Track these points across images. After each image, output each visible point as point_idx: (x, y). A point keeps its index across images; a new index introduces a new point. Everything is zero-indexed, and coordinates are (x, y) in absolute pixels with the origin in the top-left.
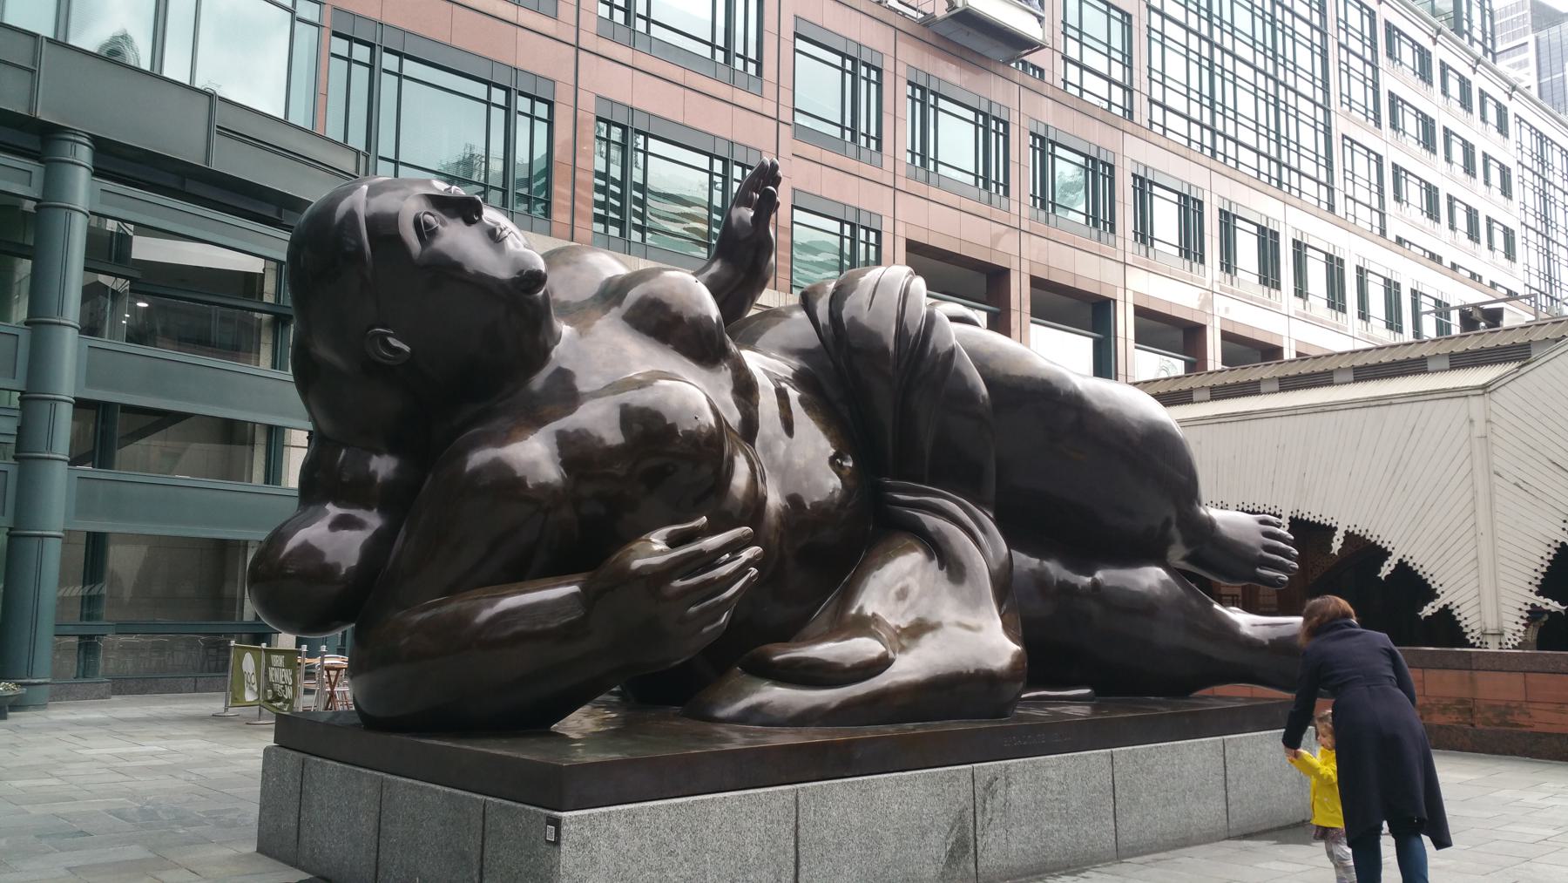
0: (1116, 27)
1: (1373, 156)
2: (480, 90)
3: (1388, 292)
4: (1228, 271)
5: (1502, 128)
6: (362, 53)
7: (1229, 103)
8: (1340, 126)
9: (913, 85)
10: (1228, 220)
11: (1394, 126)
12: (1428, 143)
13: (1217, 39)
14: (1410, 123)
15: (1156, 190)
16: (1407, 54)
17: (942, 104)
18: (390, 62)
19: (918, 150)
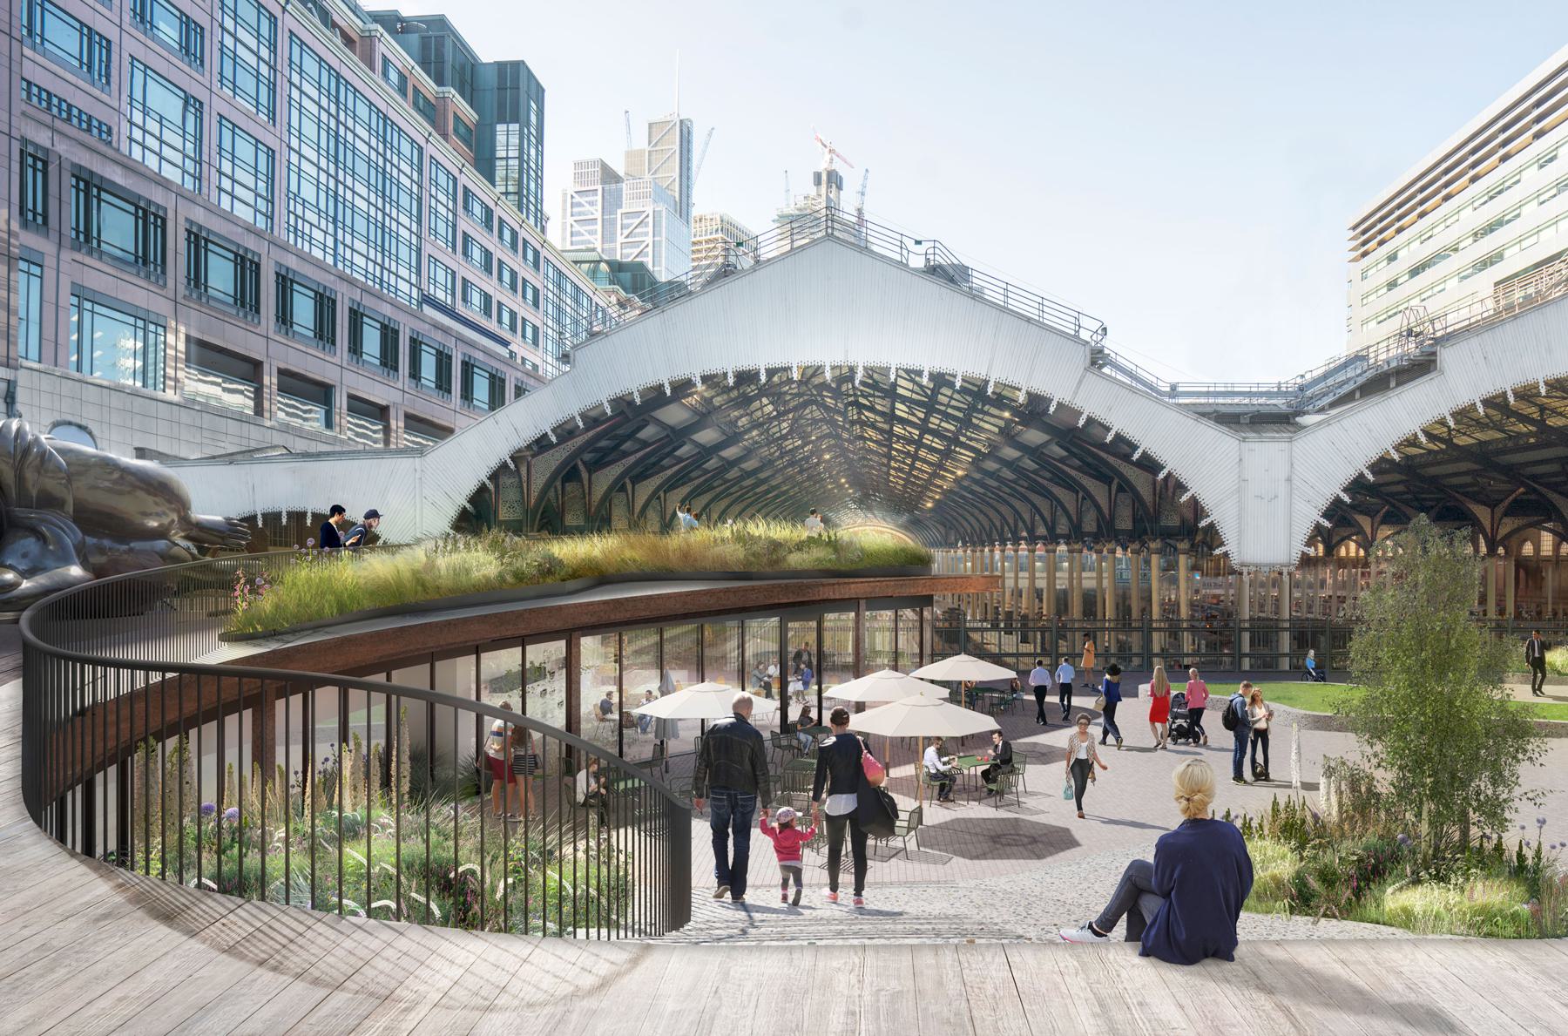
0: (262, 158)
1: (85, 31)
2: (131, 320)
3: (384, 338)
4: (355, 352)
5: (536, 265)
6: (140, 323)
7: (394, 251)
8: (428, 249)
9: (78, 179)
10: (416, 345)
11: (465, 253)
12: (488, 268)
13: (341, 178)
14: (476, 254)
15: (296, 286)
16: (477, 209)
17: (104, 195)
18: (88, 305)
19: (82, 228)
